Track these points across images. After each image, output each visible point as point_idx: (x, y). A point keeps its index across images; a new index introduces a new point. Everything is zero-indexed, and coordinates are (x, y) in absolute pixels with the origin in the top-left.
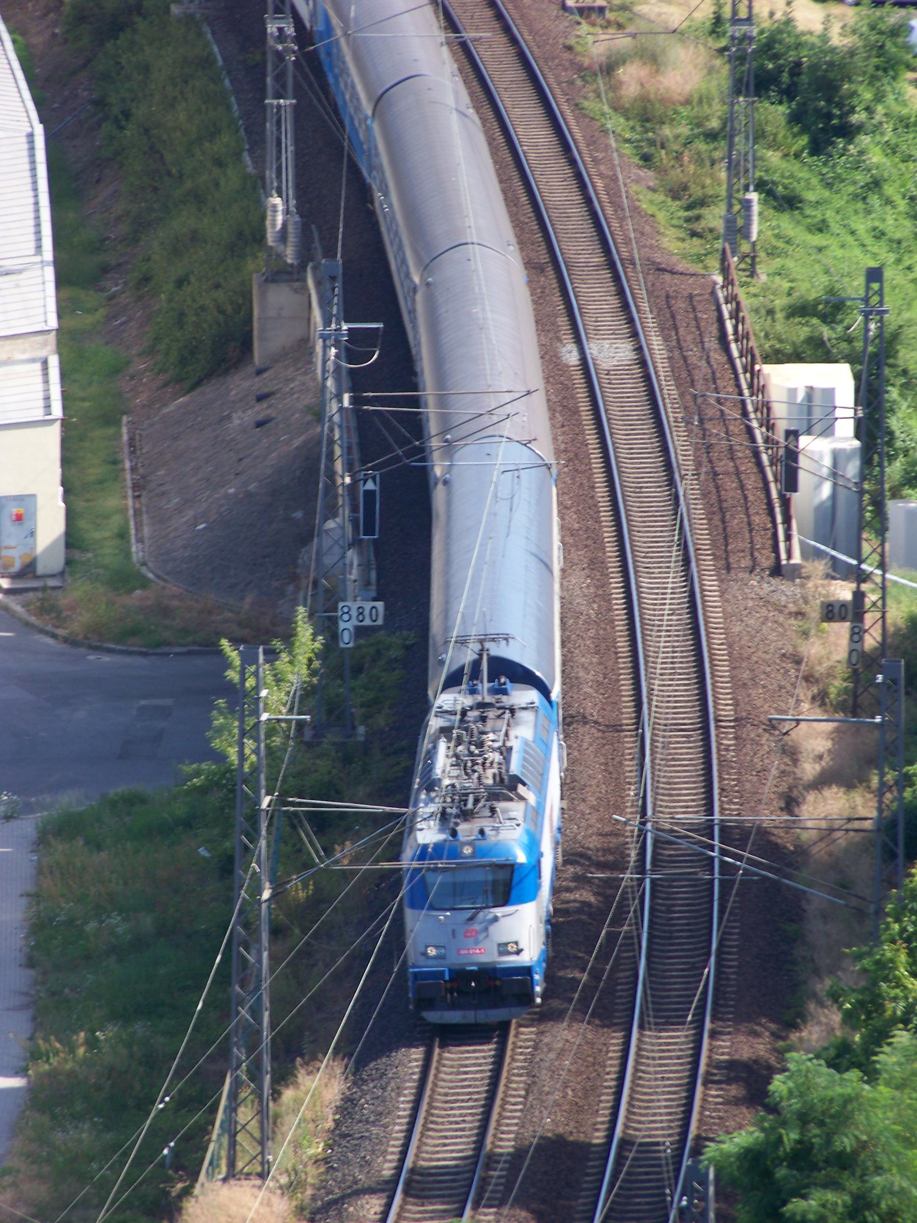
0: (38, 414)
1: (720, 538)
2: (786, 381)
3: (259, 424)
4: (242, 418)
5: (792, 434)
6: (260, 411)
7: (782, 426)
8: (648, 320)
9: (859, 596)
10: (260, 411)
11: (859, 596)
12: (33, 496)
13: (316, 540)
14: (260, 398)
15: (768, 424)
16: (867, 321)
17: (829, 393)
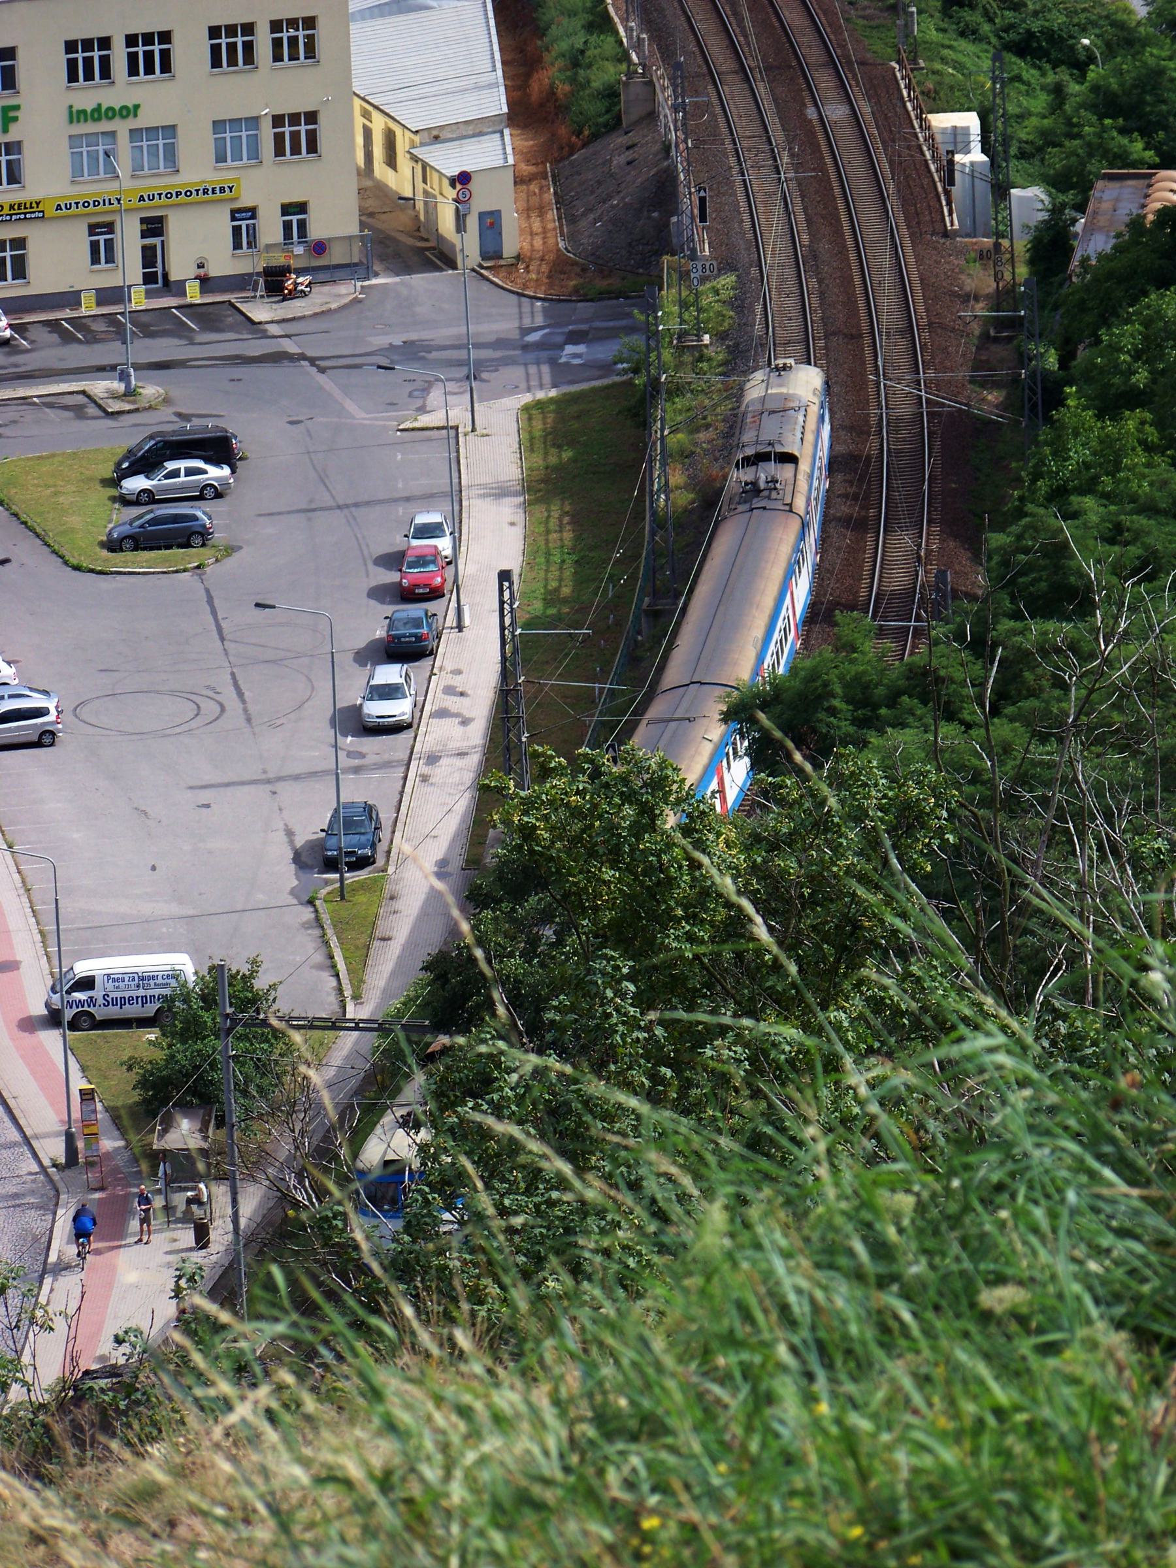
0: (500, 163)
1: (22, 891)
2: (941, 121)
3: (629, 163)
4: (619, 160)
5: (951, 153)
6: (630, 155)
7: (943, 149)
8: (856, 93)
9: (997, 246)
10: (630, 155)
11: (997, 246)
12: (499, 212)
13: (537, 434)
14: (628, 148)
15: (933, 148)
16: (994, 83)
17: (967, 129)
